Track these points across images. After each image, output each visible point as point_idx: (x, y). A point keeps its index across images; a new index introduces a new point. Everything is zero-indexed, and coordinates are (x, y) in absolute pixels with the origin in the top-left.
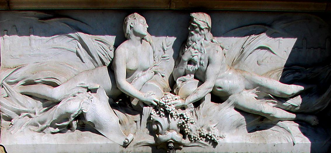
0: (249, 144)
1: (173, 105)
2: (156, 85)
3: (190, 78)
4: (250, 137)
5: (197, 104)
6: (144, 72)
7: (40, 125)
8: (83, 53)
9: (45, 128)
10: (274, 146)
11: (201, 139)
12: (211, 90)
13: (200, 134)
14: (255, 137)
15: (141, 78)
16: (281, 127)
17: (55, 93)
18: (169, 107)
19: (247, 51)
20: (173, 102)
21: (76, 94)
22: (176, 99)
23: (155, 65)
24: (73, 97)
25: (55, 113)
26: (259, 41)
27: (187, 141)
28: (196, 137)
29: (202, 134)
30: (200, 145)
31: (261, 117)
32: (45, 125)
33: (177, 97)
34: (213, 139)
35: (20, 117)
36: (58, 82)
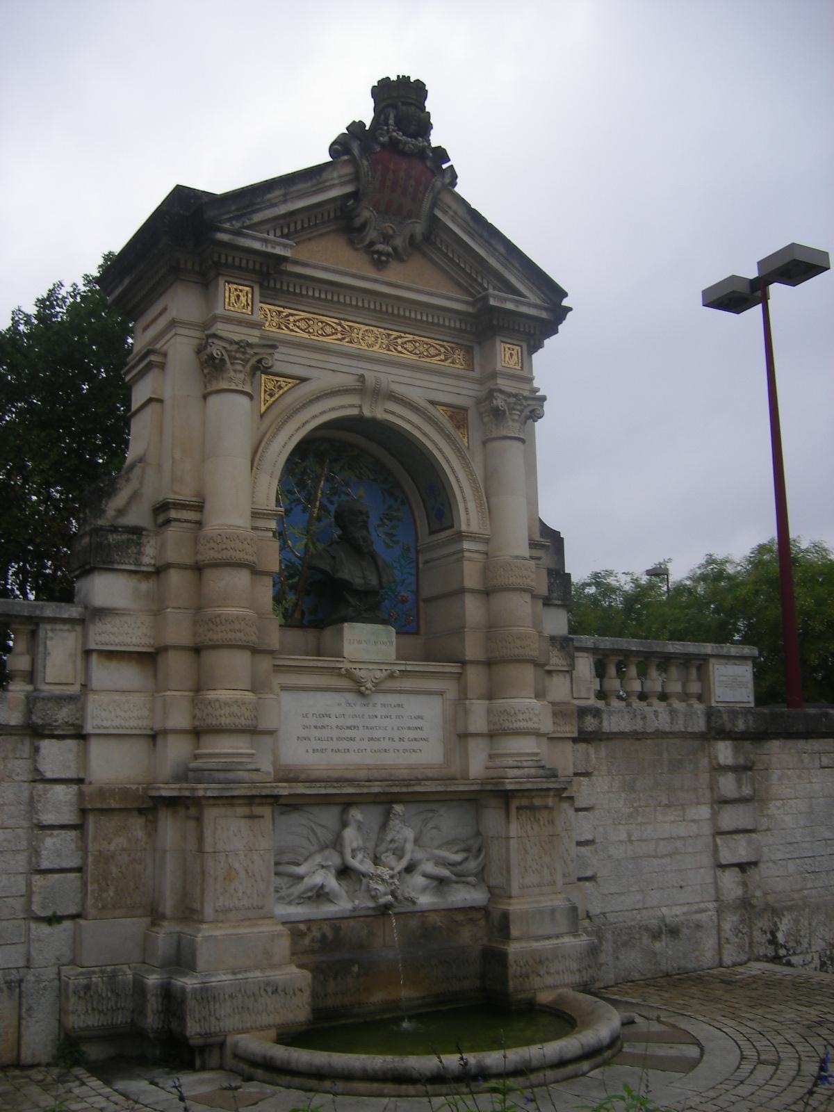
8: (311, 836)
15: (360, 856)
17: (301, 870)
25: (301, 887)
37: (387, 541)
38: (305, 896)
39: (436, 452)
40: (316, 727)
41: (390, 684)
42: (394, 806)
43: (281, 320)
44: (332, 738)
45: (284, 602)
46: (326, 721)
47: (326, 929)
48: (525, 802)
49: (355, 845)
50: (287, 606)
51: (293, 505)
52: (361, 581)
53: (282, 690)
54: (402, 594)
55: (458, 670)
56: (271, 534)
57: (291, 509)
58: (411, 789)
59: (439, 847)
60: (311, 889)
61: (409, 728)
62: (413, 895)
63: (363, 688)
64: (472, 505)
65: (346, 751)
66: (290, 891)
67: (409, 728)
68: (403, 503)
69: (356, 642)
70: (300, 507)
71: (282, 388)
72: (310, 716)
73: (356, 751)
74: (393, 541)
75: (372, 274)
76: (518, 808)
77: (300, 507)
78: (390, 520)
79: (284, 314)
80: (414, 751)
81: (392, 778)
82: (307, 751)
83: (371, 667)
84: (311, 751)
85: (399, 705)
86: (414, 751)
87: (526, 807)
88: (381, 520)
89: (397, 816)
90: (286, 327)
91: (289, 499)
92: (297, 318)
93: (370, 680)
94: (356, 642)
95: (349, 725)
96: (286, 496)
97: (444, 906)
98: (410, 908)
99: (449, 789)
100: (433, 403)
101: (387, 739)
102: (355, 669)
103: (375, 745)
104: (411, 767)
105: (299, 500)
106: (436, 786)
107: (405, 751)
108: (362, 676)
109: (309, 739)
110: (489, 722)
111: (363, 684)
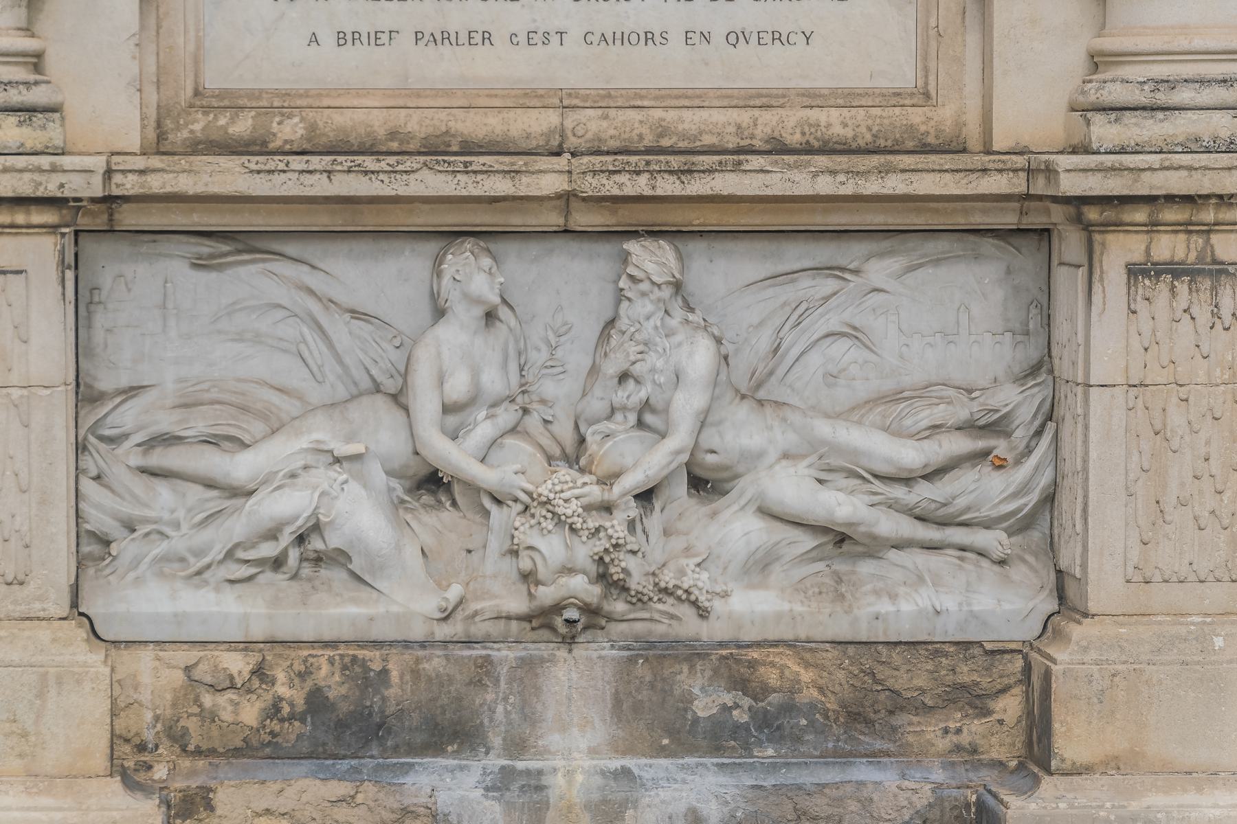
0: (800, 615)
1: (576, 498)
2: (353, 610)
3: (622, 424)
4: (803, 594)
5: (646, 496)
6: (492, 411)
7: (192, 560)
9: (208, 566)
10: (877, 618)
11: (660, 600)
12: (685, 457)
13: (656, 584)
14: (820, 593)
16: (897, 565)
18: (566, 505)
19: (795, 343)
20: (577, 492)
21: (300, 471)
22: (585, 484)
23: (524, 388)
24: (289, 480)
25: (237, 527)
26: (827, 317)
27: (619, 607)
28: (645, 591)
29: (663, 585)
30: (657, 616)
31: (836, 536)
32: (207, 560)
33: (587, 478)
34: (693, 598)
35: (135, 535)
36: (246, 438)
38: (252, 555)
47: (327, 675)
48: (1168, 247)
49: (458, 386)
58: (697, 186)
59: (853, 413)
60: (272, 535)
62: (700, 581)
65: (478, 38)
66: (206, 535)
73: (522, 38)
76: (1135, 272)
80: (776, 37)
82: (314, 39)
84: (328, 39)
86: (776, 37)
87: (1175, 270)
89: (645, 286)
97: (841, 628)
98: (689, 626)
106: (815, 175)
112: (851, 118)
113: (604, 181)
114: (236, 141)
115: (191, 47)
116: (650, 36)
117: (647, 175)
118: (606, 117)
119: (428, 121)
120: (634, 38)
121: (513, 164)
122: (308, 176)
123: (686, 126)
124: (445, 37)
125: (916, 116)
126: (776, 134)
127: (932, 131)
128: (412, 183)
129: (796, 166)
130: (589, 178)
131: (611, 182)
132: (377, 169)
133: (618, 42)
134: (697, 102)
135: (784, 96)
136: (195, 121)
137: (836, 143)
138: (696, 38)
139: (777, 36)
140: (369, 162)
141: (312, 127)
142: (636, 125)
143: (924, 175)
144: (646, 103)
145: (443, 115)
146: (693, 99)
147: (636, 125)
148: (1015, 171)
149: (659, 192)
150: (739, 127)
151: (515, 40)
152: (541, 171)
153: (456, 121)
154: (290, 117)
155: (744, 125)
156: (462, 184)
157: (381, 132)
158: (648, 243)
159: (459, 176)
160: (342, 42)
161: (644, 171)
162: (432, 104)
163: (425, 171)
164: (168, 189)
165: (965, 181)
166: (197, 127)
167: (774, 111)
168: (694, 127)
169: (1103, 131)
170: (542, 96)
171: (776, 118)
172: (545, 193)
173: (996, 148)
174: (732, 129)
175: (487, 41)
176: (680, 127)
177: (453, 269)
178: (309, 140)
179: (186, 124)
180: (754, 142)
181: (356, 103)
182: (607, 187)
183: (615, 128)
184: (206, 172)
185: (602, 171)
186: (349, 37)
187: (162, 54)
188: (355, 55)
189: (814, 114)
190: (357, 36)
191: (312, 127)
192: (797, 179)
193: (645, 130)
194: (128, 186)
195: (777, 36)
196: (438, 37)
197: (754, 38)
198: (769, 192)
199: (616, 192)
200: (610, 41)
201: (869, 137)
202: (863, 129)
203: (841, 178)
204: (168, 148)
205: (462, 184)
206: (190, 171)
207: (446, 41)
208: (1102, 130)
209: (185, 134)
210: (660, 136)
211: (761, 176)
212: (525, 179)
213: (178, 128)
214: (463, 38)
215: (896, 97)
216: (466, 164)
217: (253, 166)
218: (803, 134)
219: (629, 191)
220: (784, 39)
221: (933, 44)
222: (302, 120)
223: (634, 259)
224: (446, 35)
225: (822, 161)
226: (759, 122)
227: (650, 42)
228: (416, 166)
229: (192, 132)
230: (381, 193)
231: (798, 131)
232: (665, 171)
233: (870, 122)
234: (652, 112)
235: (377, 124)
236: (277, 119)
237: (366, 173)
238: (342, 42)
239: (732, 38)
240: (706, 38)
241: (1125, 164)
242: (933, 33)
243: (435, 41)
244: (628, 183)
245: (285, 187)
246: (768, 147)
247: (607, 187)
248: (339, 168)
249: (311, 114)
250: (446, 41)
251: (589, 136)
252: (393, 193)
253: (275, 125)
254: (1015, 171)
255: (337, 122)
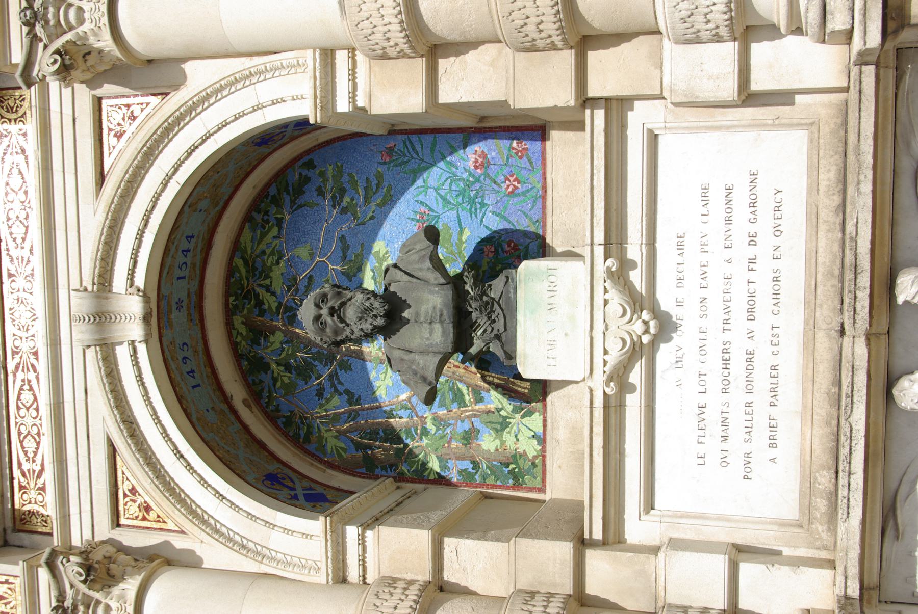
37: (379, 201)
39: (173, 189)
40: (725, 438)
41: (636, 277)
42: (900, 300)
43: (32, 485)
44: (748, 405)
45: (503, 413)
46: (713, 416)
50: (509, 408)
51: (341, 388)
52: (437, 327)
53: (652, 508)
54: (471, 164)
55: (600, 114)
56: (369, 533)
57: (347, 392)
58: (865, 263)
61: (728, 221)
63: (646, 339)
64: (265, 90)
67: (728, 221)
68: (310, 165)
69: (551, 354)
70: (343, 375)
71: (133, 488)
72: (701, 449)
73: (775, 348)
74: (378, 185)
75: (27, 101)
77: (343, 375)
78: (342, 191)
79: (22, 479)
80: (777, 209)
81: (837, 272)
82: (773, 460)
83: (599, 326)
84: (773, 453)
85: (680, 246)
86: (777, 209)
88: (344, 211)
90: (39, 476)
91: (332, 397)
92: (22, 455)
93: (628, 327)
94: (551, 354)
95: (720, 364)
96: (328, 401)
99: (868, 159)
100: (101, 178)
101: (752, 276)
102: (605, 363)
103: (764, 303)
104: (807, 411)
105: (331, 376)
107: (777, 231)
108: (620, 345)
109: (747, 455)
110: (718, 39)
111: (635, 339)
112: (825, 167)
113: (860, 317)
114: (828, 508)
115: (776, 528)
116: (775, 279)
117: (857, 292)
118: (821, 306)
119: (821, 404)
120: (776, 288)
121: (848, 370)
122: (851, 486)
123: (827, 261)
124: (773, 390)
125: (825, 130)
126: (834, 209)
127: (834, 120)
128: (858, 427)
129: (854, 205)
130: (857, 326)
131: (861, 313)
132: (848, 447)
133: (778, 296)
134: (814, 254)
135: (811, 205)
136: (817, 529)
137: (839, 175)
138: (777, 254)
139: (776, 209)
140: (844, 452)
141: (822, 467)
142: (826, 288)
143: (862, 128)
144: (813, 283)
145: (817, 395)
146: (812, 256)
147: (826, 288)
148: (861, 73)
149: (868, 285)
150: (829, 231)
151: (775, 312)
152: (853, 354)
153: (820, 388)
154: (816, 479)
155: (827, 228)
156: (859, 399)
157: (827, 430)
158: (898, 290)
159: (855, 400)
160: (774, 445)
161: (855, 294)
162: (810, 401)
163: (850, 420)
164: (857, 564)
165: (867, 103)
166: (820, 528)
167: (820, 211)
168: (828, 256)
169: (838, 22)
170: (808, 339)
171: (824, 210)
172: (866, 351)
173: (846, 85)
174: (830, 235)
175: (776, 368)
176: (828, 264)
177: (911, 403)
178: (830, 469)
179: (819, 534)
180: (838, 222)
181: (809, 442)
182: (864, 315)
183: (828, 300)
184: (847, 542)
185: (854, 318)
186: (772, 441)
187: (779, 544)
188: (782, 437)
189: (822, 188)
190: (771, 437)
191: (822, 467)
192: (862, 204)
193: (829, 284)
194: (854, 586)
195: (776, 209)
196: (773, 394)
197: (778, 222)
198: (870, 220)
199: (867, 310)
200: (777, 301)
201: (837, 157)
202: (832, 160)
203: (862, 178)
204: (832, 545)
205: (859, 399)
206: (847, 552)
207: (776, 390)
208: (838, 23)
209: (824, 535)
210: (832, 275)
211: (859, 225)
212: (857, 363)
213: (821, 538)
214: (774, 380)
215: (814, 143)
216: (847, 397)
217: (845, 516)
218: (834, 194)
219: (866, 302)
220: (778, 205)
221: (783, 121)
222: (818, 472)
223: (909, 299)
224: (772, 390)
225: (851, 190)
226: (826, 219)
227: (778, 279)
228: (848, 425)
229: (823, 531)
230: (863, 445)
231: (832, 197)
232: (855, 281)
233: (827, 156)
234: (819, 280)
235: (821, 432)
236: (817, 485)
237: (851, 453)
238: (774, 445)
239: (778, 233)
240: (777, 248)
241: (861, 7)
242: (777, 122)
243: (775, 396)
244: (862, 303)
245: (858, 499)
246: (841, 214)
247: (864, 315)
248: (847, 468)
249: (814, 467)
250: (776, 390)
251: (831, 315)
252: (863, 439)
253: (820, 487)
254: (861, 73)
255: (821, 454)
